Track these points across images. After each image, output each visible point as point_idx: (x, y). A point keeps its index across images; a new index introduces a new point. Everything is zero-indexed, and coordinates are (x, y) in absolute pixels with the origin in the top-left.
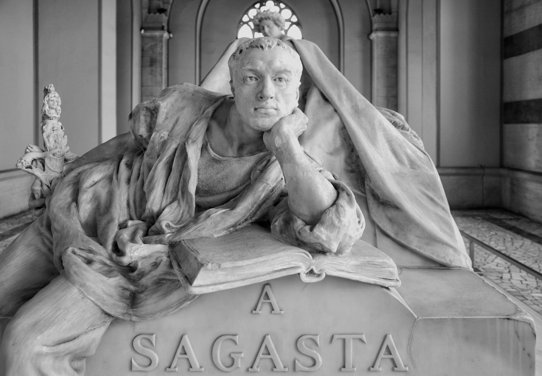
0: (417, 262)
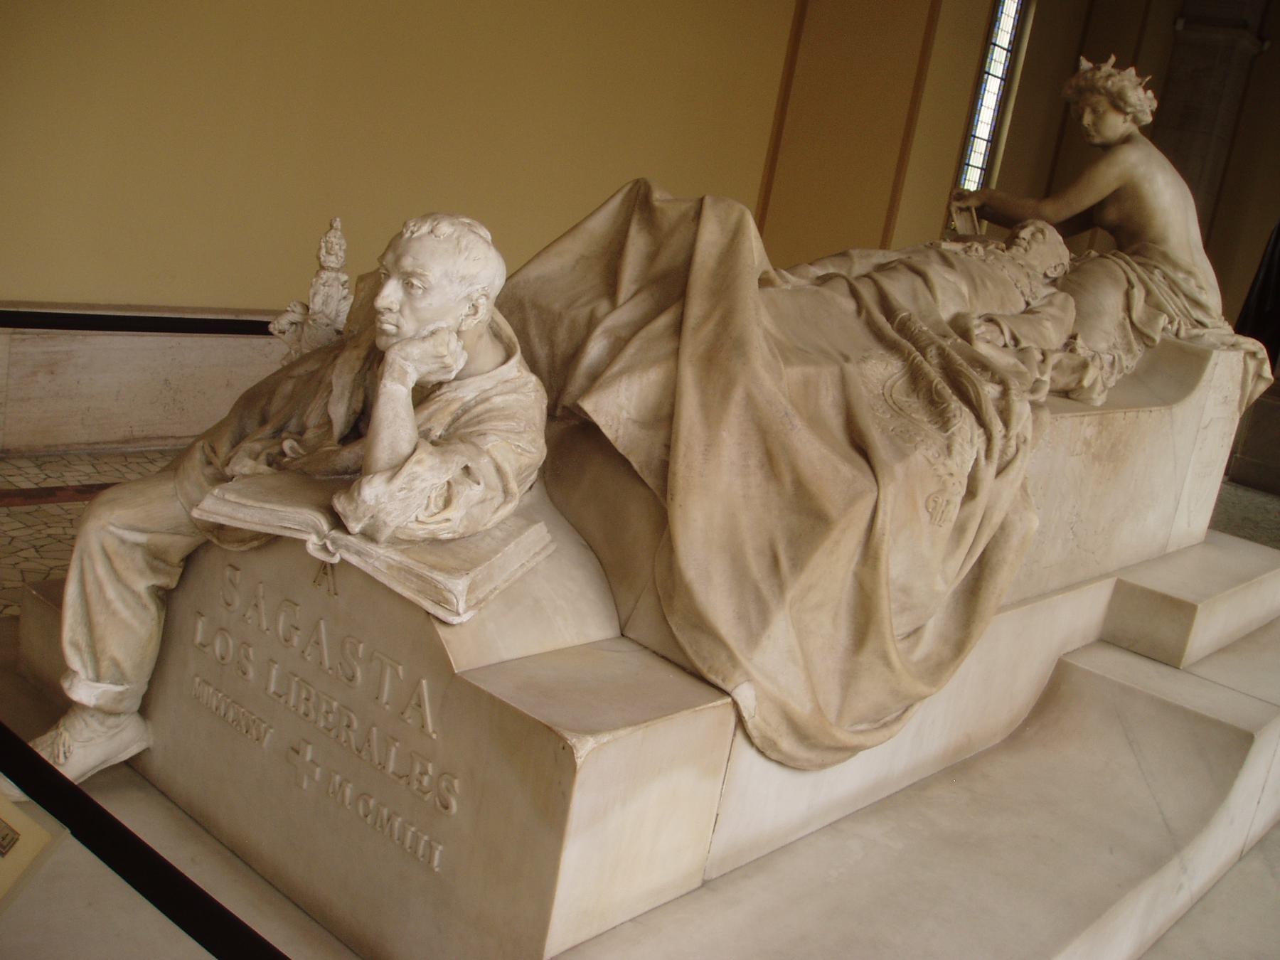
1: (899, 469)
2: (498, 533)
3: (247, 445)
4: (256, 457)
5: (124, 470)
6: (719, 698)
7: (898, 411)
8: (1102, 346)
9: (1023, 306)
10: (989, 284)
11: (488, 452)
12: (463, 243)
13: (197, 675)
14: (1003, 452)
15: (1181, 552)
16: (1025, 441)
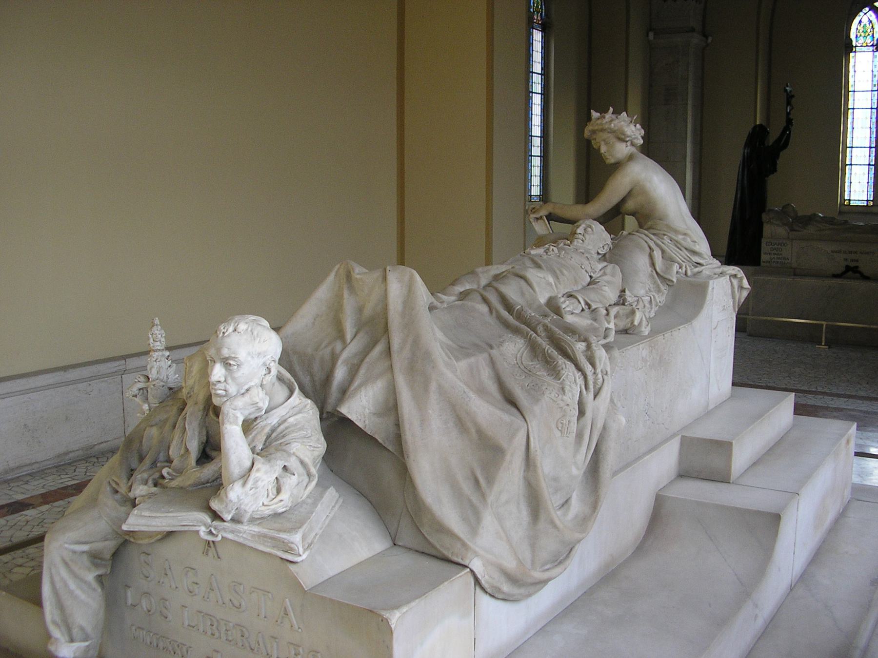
1: (537, 409)
2: (309, 501)
3: (138, 476)
4: (146, 483)
5: (11, 493)
6: (462, 571)
7: (528, 373)
8: (642, 292)
9: (588, 279)
10: (565, 272)
11: (294, 454)
12: (255, 333)
13: (132, 625)
14: (595, 383)
15: (718, 407)
16: (606, 374)
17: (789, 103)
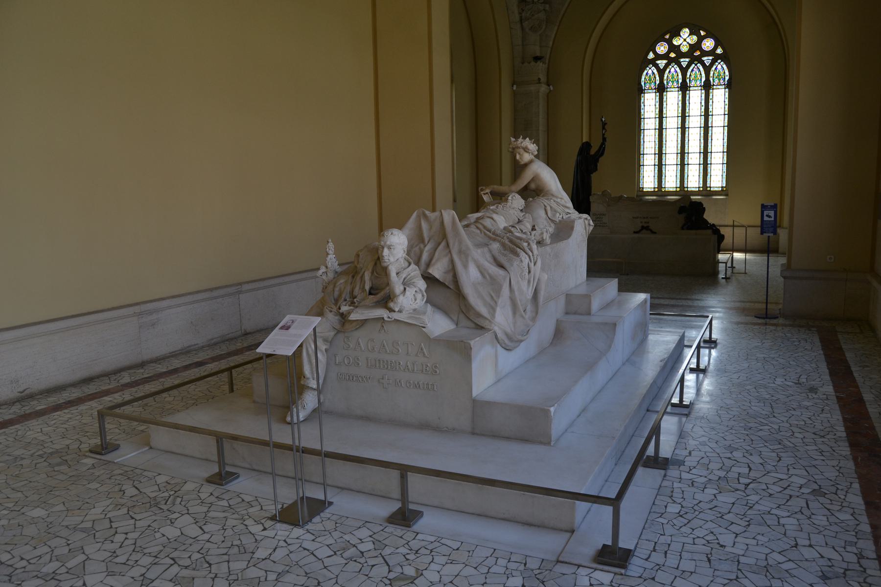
0: (473, 325)
17: (604, 128)
